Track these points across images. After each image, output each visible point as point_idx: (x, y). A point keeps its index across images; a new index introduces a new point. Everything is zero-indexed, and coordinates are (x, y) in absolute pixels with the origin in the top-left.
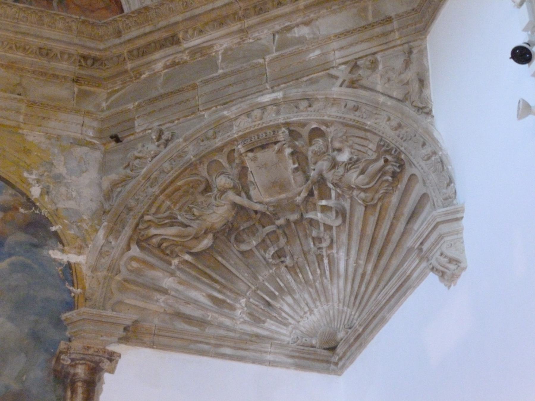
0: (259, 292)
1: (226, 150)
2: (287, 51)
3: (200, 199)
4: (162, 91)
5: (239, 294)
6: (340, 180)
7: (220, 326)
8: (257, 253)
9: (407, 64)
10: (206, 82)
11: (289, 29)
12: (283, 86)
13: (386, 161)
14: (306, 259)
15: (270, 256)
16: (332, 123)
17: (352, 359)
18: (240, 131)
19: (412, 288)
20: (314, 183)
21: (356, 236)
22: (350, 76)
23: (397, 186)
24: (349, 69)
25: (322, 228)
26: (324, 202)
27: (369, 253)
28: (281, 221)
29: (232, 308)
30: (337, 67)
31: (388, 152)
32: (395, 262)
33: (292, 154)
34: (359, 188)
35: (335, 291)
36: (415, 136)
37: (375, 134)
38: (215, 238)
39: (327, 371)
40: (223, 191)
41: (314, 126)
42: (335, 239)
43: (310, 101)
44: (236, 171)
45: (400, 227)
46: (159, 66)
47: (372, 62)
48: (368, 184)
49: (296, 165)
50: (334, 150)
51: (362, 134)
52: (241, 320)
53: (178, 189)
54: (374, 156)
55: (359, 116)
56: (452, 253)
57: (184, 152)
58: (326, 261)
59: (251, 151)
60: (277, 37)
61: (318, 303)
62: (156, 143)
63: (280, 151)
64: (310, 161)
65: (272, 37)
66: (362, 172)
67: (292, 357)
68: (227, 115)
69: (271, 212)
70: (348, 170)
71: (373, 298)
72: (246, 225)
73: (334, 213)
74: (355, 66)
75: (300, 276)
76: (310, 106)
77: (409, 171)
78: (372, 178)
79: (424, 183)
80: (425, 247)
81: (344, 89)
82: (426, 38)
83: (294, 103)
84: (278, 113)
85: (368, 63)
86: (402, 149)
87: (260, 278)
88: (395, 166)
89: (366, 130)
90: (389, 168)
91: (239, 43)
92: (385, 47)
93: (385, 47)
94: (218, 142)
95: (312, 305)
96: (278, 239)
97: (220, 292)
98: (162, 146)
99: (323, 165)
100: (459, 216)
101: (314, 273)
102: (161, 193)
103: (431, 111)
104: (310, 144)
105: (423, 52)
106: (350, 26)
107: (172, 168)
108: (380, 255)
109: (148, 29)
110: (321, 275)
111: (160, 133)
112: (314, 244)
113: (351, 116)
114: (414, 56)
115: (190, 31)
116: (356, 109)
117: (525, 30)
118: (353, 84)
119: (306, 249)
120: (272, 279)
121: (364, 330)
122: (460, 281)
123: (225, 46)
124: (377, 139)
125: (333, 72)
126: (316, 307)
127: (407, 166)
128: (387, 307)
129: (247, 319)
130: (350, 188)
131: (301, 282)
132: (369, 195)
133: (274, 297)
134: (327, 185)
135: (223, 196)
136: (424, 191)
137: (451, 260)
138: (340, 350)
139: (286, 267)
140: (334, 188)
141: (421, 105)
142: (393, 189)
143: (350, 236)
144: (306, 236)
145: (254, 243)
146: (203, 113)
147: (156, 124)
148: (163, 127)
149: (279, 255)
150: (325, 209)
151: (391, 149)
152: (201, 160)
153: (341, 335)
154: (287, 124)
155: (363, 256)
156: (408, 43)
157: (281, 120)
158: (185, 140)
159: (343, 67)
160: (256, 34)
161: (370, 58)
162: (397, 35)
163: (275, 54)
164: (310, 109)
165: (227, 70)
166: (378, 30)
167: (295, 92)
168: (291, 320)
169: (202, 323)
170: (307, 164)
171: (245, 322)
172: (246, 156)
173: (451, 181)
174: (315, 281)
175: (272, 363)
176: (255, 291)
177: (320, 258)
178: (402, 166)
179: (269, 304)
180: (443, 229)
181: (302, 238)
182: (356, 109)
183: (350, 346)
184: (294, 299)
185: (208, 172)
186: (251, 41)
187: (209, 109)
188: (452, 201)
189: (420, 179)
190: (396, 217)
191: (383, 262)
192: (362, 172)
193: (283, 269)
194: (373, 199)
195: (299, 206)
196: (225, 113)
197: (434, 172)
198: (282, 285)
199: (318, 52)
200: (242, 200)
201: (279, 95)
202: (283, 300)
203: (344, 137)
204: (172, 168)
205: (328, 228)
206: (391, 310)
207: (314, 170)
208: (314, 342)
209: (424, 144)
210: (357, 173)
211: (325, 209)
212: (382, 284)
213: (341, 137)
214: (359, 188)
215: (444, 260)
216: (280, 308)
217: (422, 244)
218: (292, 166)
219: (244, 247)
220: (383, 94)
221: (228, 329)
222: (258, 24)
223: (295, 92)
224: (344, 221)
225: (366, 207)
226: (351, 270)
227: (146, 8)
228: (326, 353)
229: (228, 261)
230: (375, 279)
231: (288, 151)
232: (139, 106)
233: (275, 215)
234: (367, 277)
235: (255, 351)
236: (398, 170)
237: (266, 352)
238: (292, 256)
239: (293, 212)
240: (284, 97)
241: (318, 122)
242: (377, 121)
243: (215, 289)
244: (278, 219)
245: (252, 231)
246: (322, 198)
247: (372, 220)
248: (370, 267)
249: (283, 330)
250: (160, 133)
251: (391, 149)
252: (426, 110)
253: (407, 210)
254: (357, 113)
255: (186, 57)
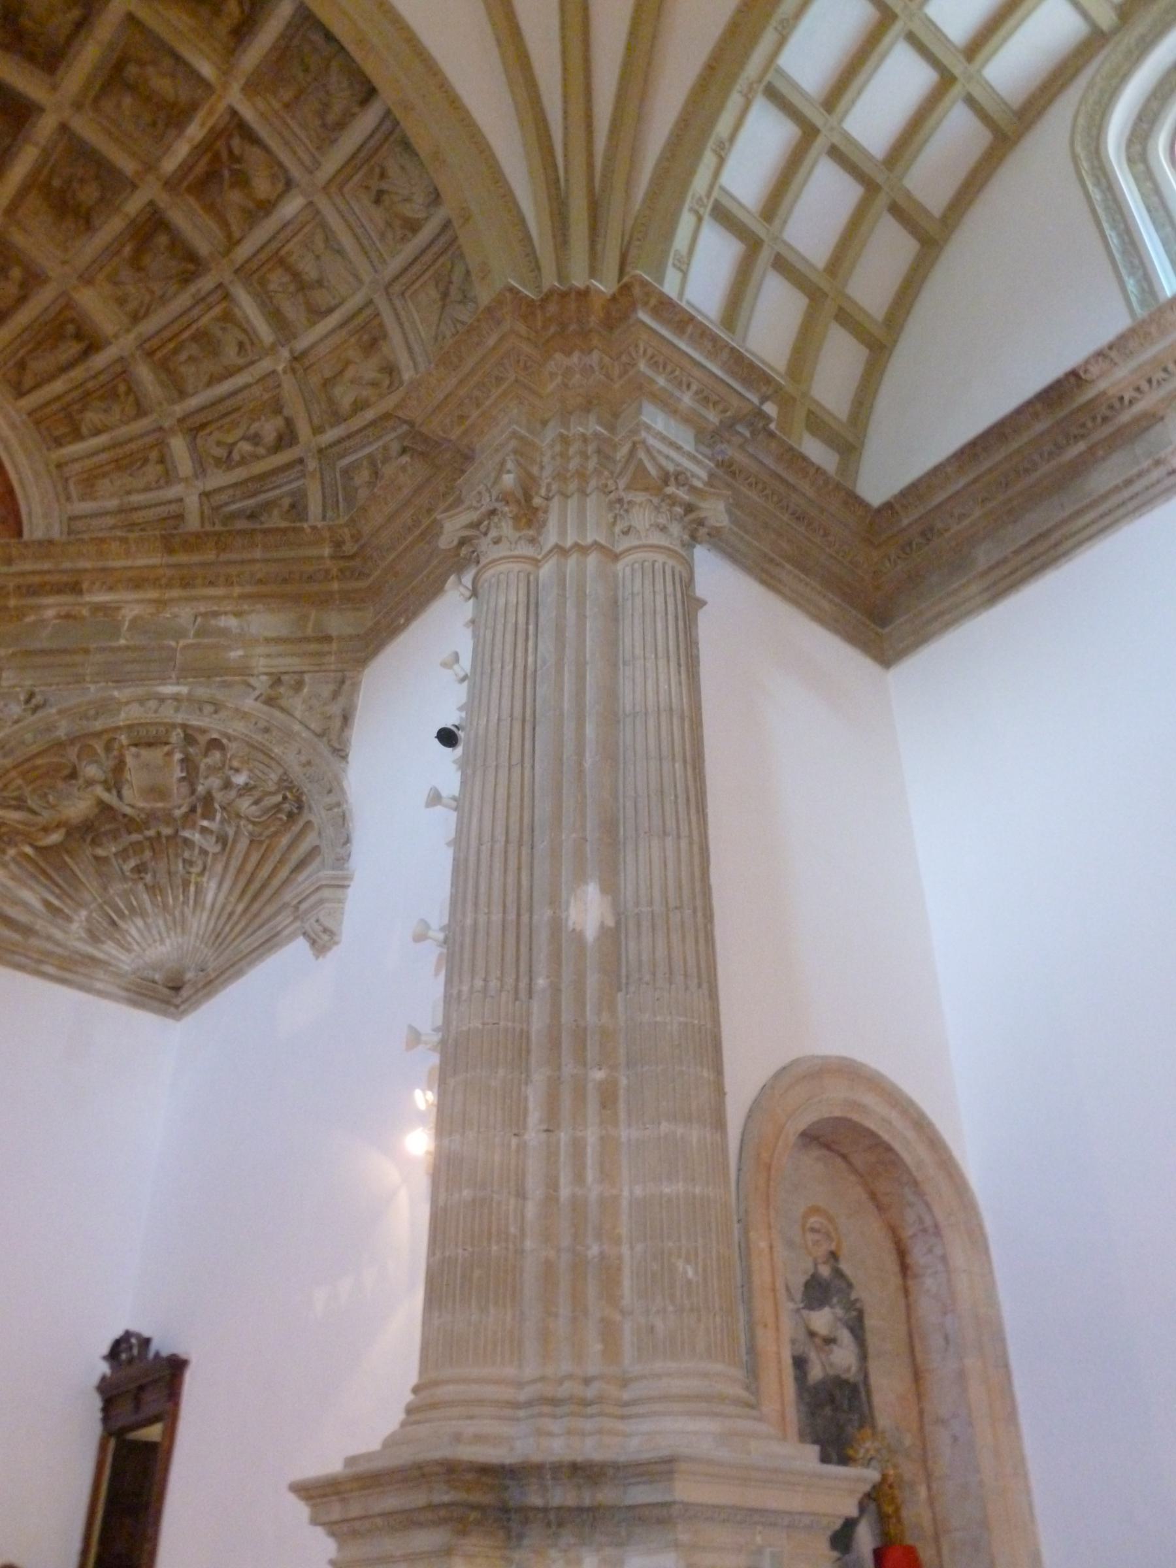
0: (106, 908)
1: (106, 737)
2: (206, 641)
3: (60, 785)
4: (46, 645)
5: (80, 905)
6: (229, 804)
7: (49, 938)
8: (113, 860)
9: (335, 695)
10: (102, 650)
11: (215, 614)
12: (191, 680)
13: (285, 798)
14: (170, 880)
15: (129, 869)
16: (236, 739)
17: (196, 1005)
18: (128, 720)
19: (280, 945)
20: (198, 799)
21: (232, 871)
22: (269, 691)
23: (290, 829)
24: (270, 683)
25: (197, 851)
26: (205, 823)
27: (243, 892)
28: (151, 833)
29: (69, 919)
30: (258, 676)
31: (290, 789)
32: (269, 910)
33: (182, 761)
34: (248, 819)
35: (195, 925)
36: (323, 779)
37: (279, 764)
38: (68, 834)
39: (165, 1013)
40: (90, 783)
41: (215, 736)
42: (208, 867)
43: (217, 707)
44: (111, 763)
45: (284, 873)
46: (50, 613)
47: (297, 683)
48: (259, 817)
49: (184, 775)
50: (231, 768)
51: (266, 760)
52: (77, 936)
53: (35, 768)
54: (273, 788)
55: (268, 740)
56: (329, 923)
57: (55, 727)
58: (192, 889)
59: (136, 745)
60: (199, 619)
61: (172, 934)
62: (23, 707)
63: (169, 754)
64: (200, 775)
65: (193, 619)
66: (256, 803)
67: (127, 990)
68: (117, 696)
69: (141, 819)
70: (240, 796)
71: (236, 943)
72: (108, 827)
73: (214, 839)
74: (277, 681)
75: (159, 898)
76: (216, 712)
77: (306, 816)
78: (265, 812)
79: (320, 834)
80: (303, 906)
81: (258, 705)
82: (363, 670)
83: (198, 705)
84: (177, 710)
85: (292, 682)
86: (305, 790)
87: (111, 891)
88: (293, 805)
89: (272, 758)
90: (286, 806)
91: (152, 614)
92: (317, 668)
93: (317, 668)
94: (98, 725)
95: (165, 935)
96: (142, 851)
97: (58, 897)
98: (29, 712)
99: (215, 782)
100: (346, 883)
101: (175, 898)
102: (15, 767)
103: (347, 755)
104: (206, 755)
105: (356, 686)
106: (284, 632)
107: (35, 742)
108: (255, 898)
109: (47, 566)
110: (184, 903)
111: (31, 695)
112: (184, 867)
113: (259, 737)
114: (346, 687)
115: (98, 584)
116: (267, 730)
117: (461, 709)
118: (270, 701)
119: (173, 869)
120: (125, 895)
121: (218, 977)
122: (330, 955)
123: (136, 612)
124: (280, 771)
125: (252, 681)
126: (169, 937)
127: (306, 811)
128: (248, 959)
129: (83, 935)
130: (238, 816)
131: (158, 906)
132: (258, 829)
133: (121, 915)
134: (213, 805)
135: (90, 789)
136: (317, 843)
137: (325, 930)
138: (185, 993)
139: (145, 885)
140: (220, 810)
141: (337, 746)
142: (285, 830)
143: (226, 867)
144: (177, 856)
145: (114, 850)
146: (89, 685)
147: (29, 682)
148: (37, 690)
149: (140, 869)
150: (204, 830)
151: (294, 787)
152: (72, 741)
153: (189, 975)
154: (184, 727)
155: (237, 892)
156: (342, 671)
157: (179, 718)
158: (60, 712)
159: (264, 678)
160: (176, 610)
161: (296, 677)
162: (333, 658)
163: (191, 641)
164: (215, 716)
165: (132, 643)
166: (313, 647)
167: (202, 692)
168: (136, 947)
169: (27, 931)
170: (197, 777)
171: (80, 939)
172: (128, 749)
173: (348, 841)
174: (174, 907)
175: (100, 993)
176: (101, 907)
177: (186, 884)
178: (300, 808)
179: (113, 923)
180: (326, 893)
181: (171, 857)
182: (267, 730)
183: (197, 991)
184: (145, 923)
185: (78, 757)
186: (168, 616)
187: (97, 682)
188: (344, 864)
189: (316, 826)
190: (282, 861)
191: (256, 906)
192: (256, 803)
193: (141, 886)
194: (260, 835)
195: (175, 820)
196: (116, 693)
197: (333, 826)
198: (135, 903)
199: (240, 653)
200: (110, 798)
201: (184, 690)
202: (132, 921)
203: (246, 758)
204: (35, 742)
205: (203, 852)
206: (251, 964)
207: (203, 784)
208: (157, 977)
209: (330, 791)
210: (251, 801)
211: (204, 830)
212: (249, 930)
213: (243, 757)
214: (248, 819)
215: (318, 928)
216: (127, 931)
217: (300, 902)
218: (179, 773)
219: (100, 852)
220: (301, 722)
221: (58, 943)
222: (180, 599)
223: (202, 692)
224: (224, 849)
225: (252, 841)
226: (218, 906)
227: (51, 542)
228: (166, 991)
229: (77, 864)
230: (243, 923)
231: (178, 756)
232: (14, 655)
233: (144, 823)
234: (235, 918)
235: (85, 975)
236: (295, 811)
237: (97, 979)
238: (154, 876)
239: (168, 824)
240: (189, 694)
241: (220, 732)
242: (286, 751)
243: (53, 893)
244: (148, 829)
245: (115, 835)
246: (204, 817)
247: (254, 858)
248: (240, 908)
249: (124, 956)
250: (31, 695)
251: (294, 787)
252: (343, 754)
253: (295, 858)
254: (266, 736)
255: (85, 612)
